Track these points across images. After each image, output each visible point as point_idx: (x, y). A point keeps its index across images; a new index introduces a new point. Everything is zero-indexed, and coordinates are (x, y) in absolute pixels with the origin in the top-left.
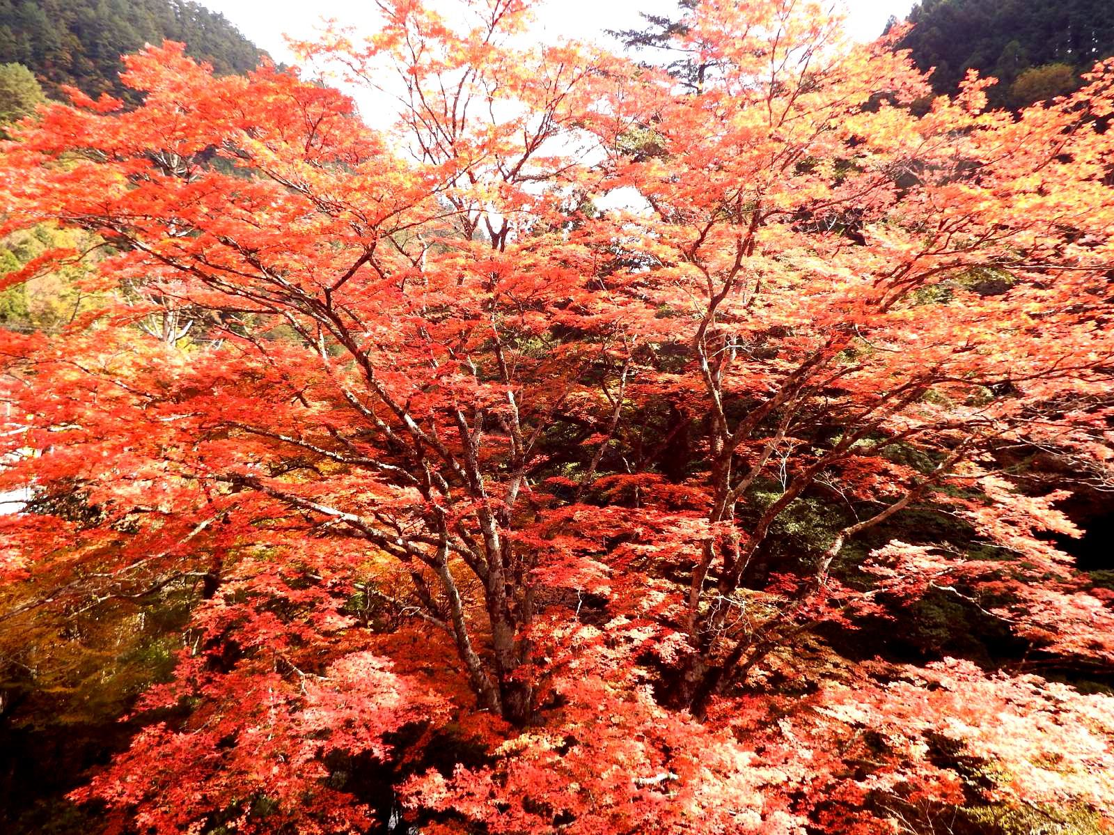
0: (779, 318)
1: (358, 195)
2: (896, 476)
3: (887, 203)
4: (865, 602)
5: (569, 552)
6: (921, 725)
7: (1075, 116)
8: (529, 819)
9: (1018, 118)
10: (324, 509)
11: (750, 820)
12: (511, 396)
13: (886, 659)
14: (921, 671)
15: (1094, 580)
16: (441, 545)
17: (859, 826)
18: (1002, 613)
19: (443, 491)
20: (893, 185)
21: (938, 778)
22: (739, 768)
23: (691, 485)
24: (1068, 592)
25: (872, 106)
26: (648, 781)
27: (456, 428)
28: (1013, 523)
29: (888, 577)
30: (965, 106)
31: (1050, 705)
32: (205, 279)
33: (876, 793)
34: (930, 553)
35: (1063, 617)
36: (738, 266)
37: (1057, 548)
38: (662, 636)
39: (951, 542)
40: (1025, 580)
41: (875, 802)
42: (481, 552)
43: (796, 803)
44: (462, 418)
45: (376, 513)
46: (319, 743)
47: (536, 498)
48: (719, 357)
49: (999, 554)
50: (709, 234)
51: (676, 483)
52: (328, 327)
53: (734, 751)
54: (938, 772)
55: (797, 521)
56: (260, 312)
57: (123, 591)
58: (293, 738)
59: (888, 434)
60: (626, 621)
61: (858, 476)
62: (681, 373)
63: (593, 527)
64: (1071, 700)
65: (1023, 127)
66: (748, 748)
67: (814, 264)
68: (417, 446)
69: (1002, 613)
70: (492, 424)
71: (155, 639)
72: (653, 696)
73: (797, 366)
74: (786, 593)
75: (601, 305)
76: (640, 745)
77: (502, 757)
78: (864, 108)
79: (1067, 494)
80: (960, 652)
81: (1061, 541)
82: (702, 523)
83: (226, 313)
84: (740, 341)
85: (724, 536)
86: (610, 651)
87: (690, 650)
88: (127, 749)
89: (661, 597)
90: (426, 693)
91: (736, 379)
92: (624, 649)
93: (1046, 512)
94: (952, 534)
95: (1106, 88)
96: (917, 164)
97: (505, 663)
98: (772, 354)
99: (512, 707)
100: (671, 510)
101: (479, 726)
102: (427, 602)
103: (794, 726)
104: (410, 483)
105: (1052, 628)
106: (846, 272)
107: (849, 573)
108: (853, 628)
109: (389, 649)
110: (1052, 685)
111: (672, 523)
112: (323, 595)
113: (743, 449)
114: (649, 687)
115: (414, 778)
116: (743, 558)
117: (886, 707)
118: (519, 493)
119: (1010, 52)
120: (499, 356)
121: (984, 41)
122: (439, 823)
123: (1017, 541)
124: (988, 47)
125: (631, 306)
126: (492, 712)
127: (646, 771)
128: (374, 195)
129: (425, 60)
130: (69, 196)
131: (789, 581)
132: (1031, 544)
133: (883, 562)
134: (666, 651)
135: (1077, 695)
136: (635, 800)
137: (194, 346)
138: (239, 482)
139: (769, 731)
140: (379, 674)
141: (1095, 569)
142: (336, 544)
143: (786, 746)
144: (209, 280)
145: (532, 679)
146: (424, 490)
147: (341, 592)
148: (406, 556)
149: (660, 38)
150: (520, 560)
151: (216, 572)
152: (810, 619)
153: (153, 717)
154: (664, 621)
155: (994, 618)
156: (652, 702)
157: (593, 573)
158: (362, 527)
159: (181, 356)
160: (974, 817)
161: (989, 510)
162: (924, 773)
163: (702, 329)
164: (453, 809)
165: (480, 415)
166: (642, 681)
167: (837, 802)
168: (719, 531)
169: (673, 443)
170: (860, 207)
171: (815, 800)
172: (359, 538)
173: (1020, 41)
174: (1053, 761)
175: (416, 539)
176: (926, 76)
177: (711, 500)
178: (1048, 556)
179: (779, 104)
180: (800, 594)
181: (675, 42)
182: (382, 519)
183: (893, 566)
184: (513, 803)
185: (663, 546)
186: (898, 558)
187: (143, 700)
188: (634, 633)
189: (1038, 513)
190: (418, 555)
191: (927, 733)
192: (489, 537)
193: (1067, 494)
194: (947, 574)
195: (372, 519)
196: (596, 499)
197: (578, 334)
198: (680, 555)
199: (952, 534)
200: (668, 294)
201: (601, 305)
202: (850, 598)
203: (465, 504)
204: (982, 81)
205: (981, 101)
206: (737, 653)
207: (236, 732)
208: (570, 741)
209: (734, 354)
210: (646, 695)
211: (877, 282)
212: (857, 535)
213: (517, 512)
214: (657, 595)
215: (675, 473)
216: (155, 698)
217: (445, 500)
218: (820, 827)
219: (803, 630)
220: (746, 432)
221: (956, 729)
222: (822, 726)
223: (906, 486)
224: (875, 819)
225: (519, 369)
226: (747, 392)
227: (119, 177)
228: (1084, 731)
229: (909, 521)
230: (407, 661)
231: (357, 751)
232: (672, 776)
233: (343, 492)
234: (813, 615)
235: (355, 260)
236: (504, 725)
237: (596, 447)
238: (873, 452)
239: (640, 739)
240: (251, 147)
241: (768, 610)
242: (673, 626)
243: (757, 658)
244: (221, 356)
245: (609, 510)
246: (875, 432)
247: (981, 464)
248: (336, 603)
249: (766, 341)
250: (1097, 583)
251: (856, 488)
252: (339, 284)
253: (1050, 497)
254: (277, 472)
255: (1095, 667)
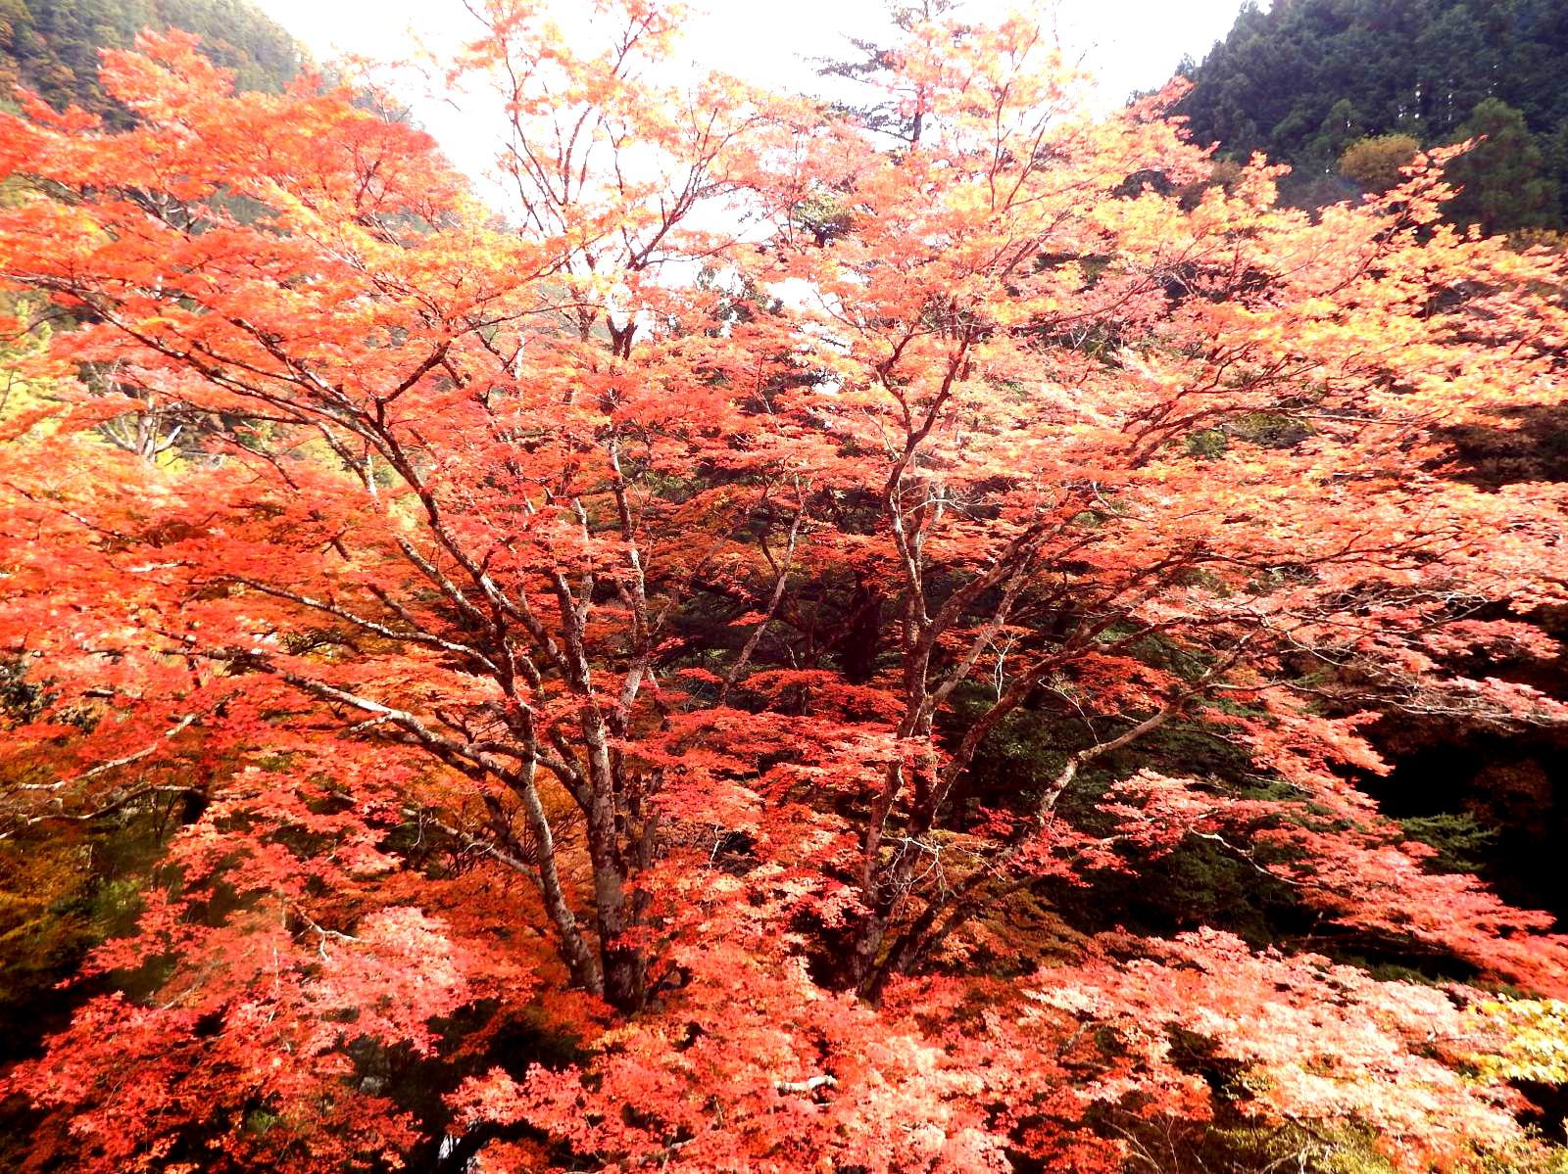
0: (995, 468)
1: (428, 276)
2: (1150, 685)
3: (1152, 317)
4: (1101, 853)
5: (704, 771)
6: (1162, 1016)
7: (1390, 220)
8: (630, 1134)
9: (1315, 220)
10: (362, 703)
11: (929, 1139)
12: (635, 555)
13: (1130, 930)
14: (1169, 945)
15: (1406, 831)
16: (526, 758)
17: (1075, 1149)
18: (1282, 871)
19: (533, 683)
20: (1163, 291)
21: (1181, 1086)
22: (921, 1069)
23: (879, 687)
24: (1371, 846)
25: (1130, 188)
26: (797, 1086)
27: (555, 597)
28: (1303, 753)
29: (1132, 820)
30: (1249, 199)
31: (1334, 994)
32: (204, 371)
33: (1099, 1105)
34: (1193, 788)
35: (1359, 878)
36: (945, 394)
37: (1359, 788)
38: (826, 890)
39: (1219, 776)
40: (1318, 829)
41: (1101, 1119)
42: (583, 771)
43: (994, 1117)
44: (564, 585)
45: (438, 713)
46: (341, 1029)
47: (664, 697)
48: (919, 514)
49: (1289, 793)
50: (905, 351)
51: (854, 683)
52: (380, 448)
53: (915, 1047)
54: (1181, 1078)
55: (1021, 740)
56: (284, 420)
57: (66, 811)
58: (304, 1018)
59: (1140, 624)
60: (778, 870)
61: (1101, 681)
62: (871, 533)
63: (742, 740)
64: (1361, 988)
65: (1321, 232)
66: (936, 1045)
67: (1052, 392)
68: (497, 619)
69: (1282, 871)
70: (605, 592)
71: (108, 881)
72: (808, 971)
73: (1023, 529)
74: (998, 836)
75: (764, 437)
76: (788, 1038)
77: (600, 1053)
78: (1117, 193)
79: (1376, 716)
80: (1223, 921)
81: (1363, 778)
82: (889, 740)
83: (231, 418)
84: (947, 495)
85: (917, 757)
86: (755, 909)
87: (862, 910)
88: (67, 1027)
89: (827, 837)
90: (497, 962)
91: (943, 543)
92: (772, 908)
93: (1346, 739)
94: (1222, 765)
95: (1429, 187)
96: (1190, 269)
97: (611, 923)
98: (994, 513)
99: (619, 985)
100: (848, 720)
101: (569, 1011)
102: (506, 841)
103: (1003, 1018)
104: (487, 671)
105: (1344, 891)
106: (1095, 408)
107: (1078, 811)
108: (1084, 885)
109: (448, 901)
110: (1340, 968)
111: (849, 739)
112: (356, 823)
113: (949, 638)
114: (803, 962)
115: (470, 1081)
116: (941, 787)
117: (1124, 991)
118: (641, 689)
119: (1338, 115)
120: (620, 498)
121: (1306, 97)
122: (503, 1142)
123: (1301, 774)
124: (1312, 105)
125: (806, 440)
126: (590, 991)
127: (791, 1072)
128: (450, 278)
129: (531, 91)
130: (18, 248)
131: (1002, 819)
132: (1325, 781)
133: (1127, 799)
134: (830, 911)
135: (1370, 981)
136: (777, 1109)
137: (181, 462)
138: (242, 661)
139: (969, 1024)
140: (429, 938)
141: (1408, 816)
142: (373, 753)
143: (990, 1044)
144: (211, 375)
145: (647, 946)
146: (505, 682)
147: (382, 820)
148: (478, 773)
149: (866, 69)
150: (630, 782)
151: (204, 787)
152: (1026, 873)
153: (104, 983)
154: (829, 870)
155: (1273, 878)
156: (806, 978)
157: (738, 805)
158: (413, 729)
159: (165, 476)
160: (1231, 1140)
161: (1272, 734)
162: (1164, 1078)
163: (895, 476)
164: (524, 1122)
165: (589, 579)
166: (796, 950)
167: (1049, 1117)
168: (908, 751)
169: (848, 629)
170: (1117, 319)
171: (1020, 1113)
172: (412, 744)
173: (1352, 100)
174: (1324, 1065)
175: (493, 748)
176: (1207, 153)
177: (903, 707)
178: (1350, 803)
179: (1006, 182)
180: (1012, 840)
181: (883, 75)
182: (445, 720)
183: (1141, 804)
184: (607, 1113)
185: (834, 769)
186: (1149, 794)
187: (93, 959)
188: (788, 887)
189: (1335, 739)
190: (494, 770)
191: (1169, 1026)
192: (594, 748)
193: (1376, 716)
194: (1212, 816)
195: (432, 720)
196: (752, 703)
197: (733, 475)
198: (857, 781)
199: (1222, 765)
200: (855, 424)
201: (764, 437)
202: (1083, 846)
203: (562, 702)
204: (1271, 169)
205: (1270, 193)
206: (927, 919)
207: (224, 1009)
208: (694, 1030)
209: (940, 510)
210: (798, 968)
211: (1127, 425)
212: (1100, 761)
213: (636, 715)
214: (823, 835)
215: (857, 669)
216: (110, 958)
217: (534, 696)
218: (1024, 1150)
219: (1019, 887)
220: (951, 616)
221: (1208, 1023)
222: (1033, 1015)
223: (1165, 697)
224: (1098, 1140)
225: (647, 517)
226: (958, 563)
227: (91, 228)
228: (1371, 1027)
229: (1173, 745)
230: (476, 920)
231: (392, 1041)
232: (831, 1080)
233: (391, 680)
234: (1031, 868)
235: (420, 359)
236: (606, 1009)
237: (754, 627)
238: (1117, 650)
239: (787, 1029)
240: (281, 201)
241: (976, 860)
242: (845, 878)
243: (956, 921)
244: (221, 477)
245: (764, 717)
246: (1122, 621)
247: (1264, 673)
248: (374, 837)
249: (985, 497)
250: (1410, 835)
251: (1096, 698)
252: (397, 393)
253: (1353, 719)
254: (298, 649)
255: (1401, 947)
